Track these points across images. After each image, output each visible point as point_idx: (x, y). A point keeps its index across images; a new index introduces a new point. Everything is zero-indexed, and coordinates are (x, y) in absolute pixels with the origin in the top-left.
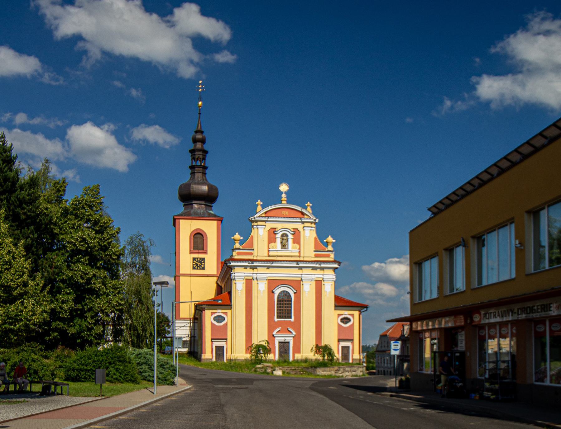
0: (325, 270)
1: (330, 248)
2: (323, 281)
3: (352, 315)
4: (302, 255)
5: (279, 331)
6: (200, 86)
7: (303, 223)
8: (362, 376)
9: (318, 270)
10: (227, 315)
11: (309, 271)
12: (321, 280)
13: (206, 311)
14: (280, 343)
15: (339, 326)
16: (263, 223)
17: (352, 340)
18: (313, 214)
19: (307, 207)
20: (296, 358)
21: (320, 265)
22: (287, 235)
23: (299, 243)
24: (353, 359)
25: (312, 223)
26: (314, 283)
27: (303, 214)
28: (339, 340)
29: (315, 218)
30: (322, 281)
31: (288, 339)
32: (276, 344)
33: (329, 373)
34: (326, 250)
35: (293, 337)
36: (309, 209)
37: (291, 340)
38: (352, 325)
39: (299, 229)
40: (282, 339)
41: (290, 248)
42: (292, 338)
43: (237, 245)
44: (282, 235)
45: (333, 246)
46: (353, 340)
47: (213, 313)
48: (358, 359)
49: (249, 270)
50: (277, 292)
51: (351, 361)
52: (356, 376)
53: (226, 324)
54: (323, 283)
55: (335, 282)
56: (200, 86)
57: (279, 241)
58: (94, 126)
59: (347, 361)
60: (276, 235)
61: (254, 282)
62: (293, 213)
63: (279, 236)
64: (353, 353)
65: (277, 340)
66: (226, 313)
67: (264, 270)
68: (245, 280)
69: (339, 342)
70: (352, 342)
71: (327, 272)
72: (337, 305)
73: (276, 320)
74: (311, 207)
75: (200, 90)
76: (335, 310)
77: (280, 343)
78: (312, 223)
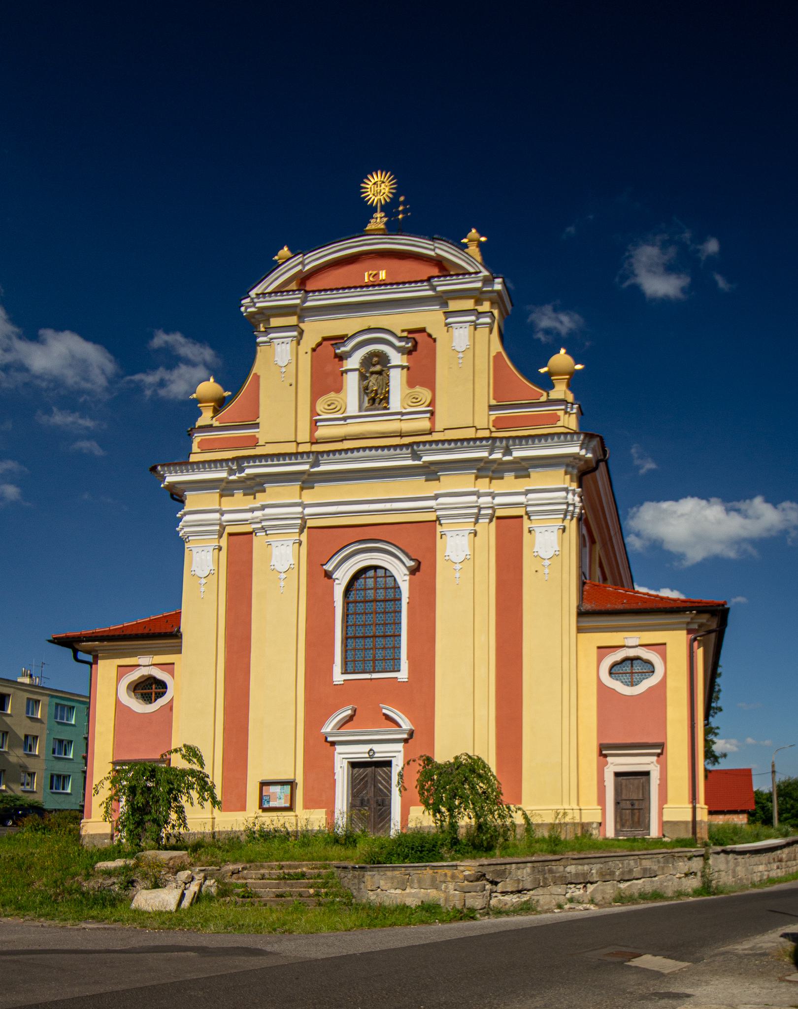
0: (534, 473)
1: (560, 391)
2: (529, 518)
3: (659, 648)
4: (439, 426)
5: (351, 718)
6: (401, 208)
7: (442, 299)
8: (696, 893)
9: (509, 477)
10: (172, 674)
11: (464, 482)
12: (521, 517)
13: (99, 661)
14: (354, 765)
15: (603, 691)
16: (293, 320)
17: (659, 748)
18: (487, 262)
19: (465, 246)
20: (412, 825)
21: (508, 451)
22: (383, 359)
23: (430, 383)
24: (663, 824)
25: (478, 296)
26: (488, 531)
27: (443, 267)
28: (604, 750)
29: (485, 273)
30: (525, 517)
31: (382, 751)
32: (338, 770)
33: (432, 894)
34: (544, 398)
35: (406, 741)
36: (474, 250)
37: (396, 754)
38: (660, 690)
39: (429, 330)
40: (360, 752)
41: (396, 403)
42: (400, 746)
43: (206, 418)
44: (367, 361)
45: (570, 386)
46: (662, 746)
47: (123, 670)
48: (686, 823)
49: (239, 500)
50: (343, 576)
51: (654, 832)
52: (657, 895)
53: (171, 703)
54: (527, 524)
55: (582, 520)
56: (401, 208)
57: (352, 382)
58: (195, 344)
59: (639, 834)
60: (345, 361)
61: (258, 541)
62: (407, 269)
63: (354, 362)
64: (663, 799)
65: (342, 758)
66: (169, 667)
67: (289, 493)
68: (225, 535)
69: (602, 755)
70: (659, 755)
71: (539, 479)
72: (587, 606)
73: (338, 677)
74: (480, 245)
75: (400, 217)
76: (580, 630)
77: (354, 765)
78: (478, 296)
